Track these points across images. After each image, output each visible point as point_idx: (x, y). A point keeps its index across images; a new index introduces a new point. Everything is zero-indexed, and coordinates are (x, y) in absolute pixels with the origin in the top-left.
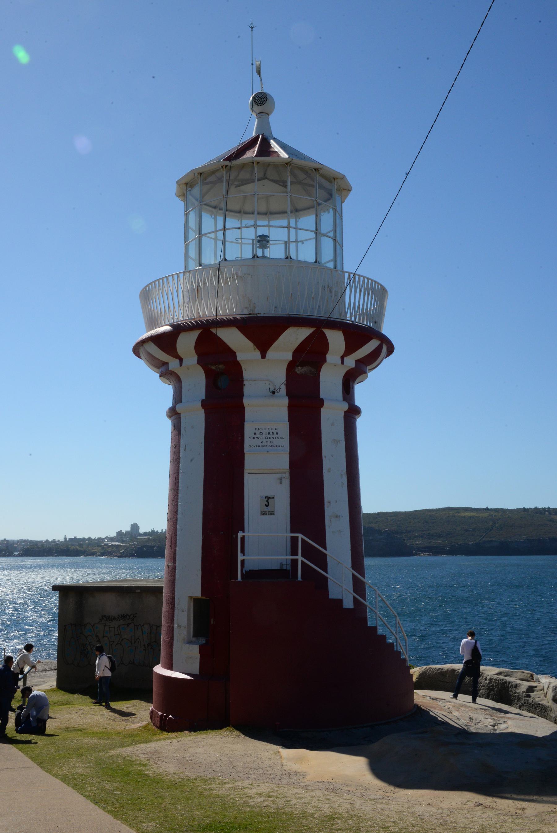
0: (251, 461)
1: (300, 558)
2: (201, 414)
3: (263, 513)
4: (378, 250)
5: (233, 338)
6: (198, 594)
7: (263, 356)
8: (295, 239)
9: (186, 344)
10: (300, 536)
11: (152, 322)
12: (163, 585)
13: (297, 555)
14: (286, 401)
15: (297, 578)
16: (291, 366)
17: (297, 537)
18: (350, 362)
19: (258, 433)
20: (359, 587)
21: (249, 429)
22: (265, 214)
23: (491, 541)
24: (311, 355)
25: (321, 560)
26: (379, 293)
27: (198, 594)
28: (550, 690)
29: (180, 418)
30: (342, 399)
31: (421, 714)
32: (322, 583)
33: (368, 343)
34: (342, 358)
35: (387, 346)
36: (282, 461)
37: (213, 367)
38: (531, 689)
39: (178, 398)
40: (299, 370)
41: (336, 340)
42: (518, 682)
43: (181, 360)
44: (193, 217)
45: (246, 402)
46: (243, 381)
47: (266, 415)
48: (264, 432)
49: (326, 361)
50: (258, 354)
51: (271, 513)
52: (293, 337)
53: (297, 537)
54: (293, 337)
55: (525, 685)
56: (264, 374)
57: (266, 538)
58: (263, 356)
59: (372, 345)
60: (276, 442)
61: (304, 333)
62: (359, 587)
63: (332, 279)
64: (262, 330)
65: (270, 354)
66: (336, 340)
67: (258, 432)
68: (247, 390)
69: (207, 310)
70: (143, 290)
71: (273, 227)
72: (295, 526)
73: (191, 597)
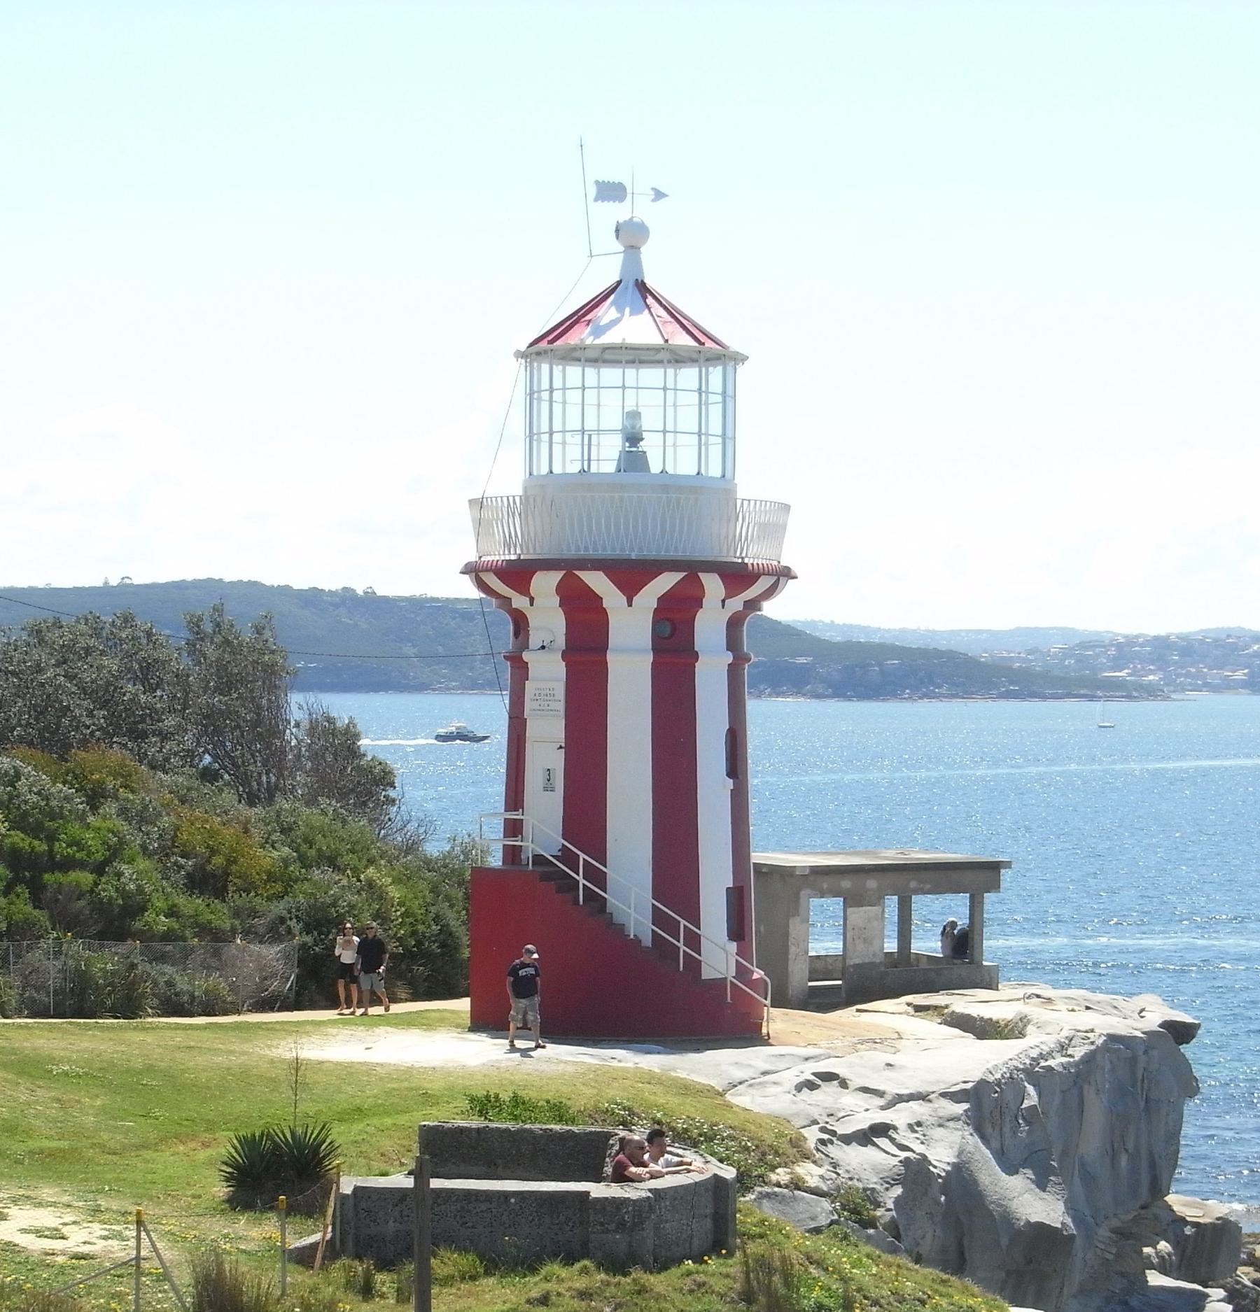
3: (546, 789)
5: (597, 582)
7: (630, 605)
34: (723, 601)
41: (713, 585)
43: (532, 600)
52: (665, 582)
54: (665, 582)
56: (630, 624)
58: (630, 605)
64: (631, 576)
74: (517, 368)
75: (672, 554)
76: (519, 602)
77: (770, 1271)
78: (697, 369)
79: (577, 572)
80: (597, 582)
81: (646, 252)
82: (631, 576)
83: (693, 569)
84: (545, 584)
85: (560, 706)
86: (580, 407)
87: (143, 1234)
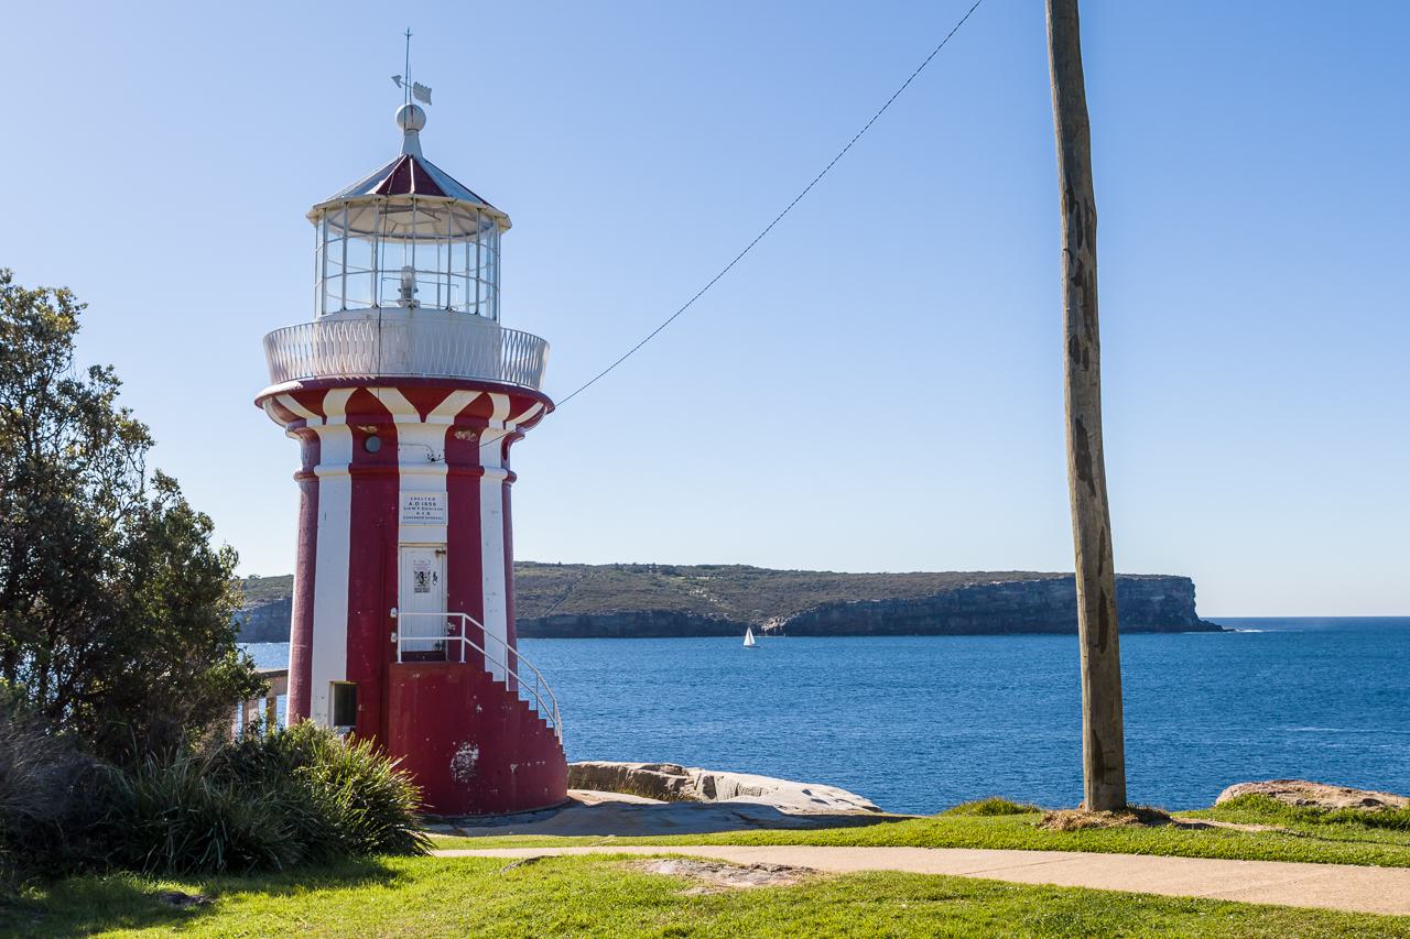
0: (405, 533)
1: (464, 639)
2: (347, 479)
3: (417, 591)
4: (540, 295)
5: (391, 399)
6: (342, 678)
7: (423, 420)
8: (440, 272)
9: (336, 402)
10: (464, 616)
11: (279, 372)
12: (1074, 570)
13: (460, 635)
14: (445, 469)
15: (460, 659)
16: (451, 431)
17: (461, 617)
18: (512, 426)
19: (414, 502)
20: (512, 661)
21: (404, 498)
22: (402, 237)
23: (564, 615)
24: (475, 419)
25: (476, 635)
26: (537, 346)
27: (342, 678)
28: (701, 781)
29: (318, 482)
30: (500, 466)
31: (573, 803)
32: (476, 659)
33: (527, 402)
34: (505, 422)
35: (549, 405)
36: (440, 535)
37: (364, 429)
38: (680, 783)
39: (313, 455)
40: (460, 435)
41: (502, 404)
42: (666, 775)
43: (325, 418)
44: (335, 250)
45: (401, 468)
46: (397, 444)
47: (422, 484)
48: (420, 502)
49: (488, 426)
50: (417, 417)
51: (426, 591)
52: (460, 400)
53: (461, 617)
54: (460, 400)
55: (672, 779)
56: (421, 440)
57: (419, 618)
58: (423, 420)
59: (538, 406)
60: (433, 513)
61: (469, 397)
62: (512, 661)
63: (484, 328)
64: (426, 394)
65: (430, 417)
66: (502, 404)
67: (414, 502)
68: (401, 455)
69: (356, 365)
70: (268, 335)
71: (439, 288)
72: (452, 605)
73: (332, 683)
74: (310, 234)
75: (467, 376)
76: (313, 421)
77: (228, 641)
78: (464, 245)
79: (373, 391)
80: (391, 399)
81: (423, 135)
82: (426, 394)
83: (486, 388)
84: (336, 402)
85: (444, 514)
86: (348, 297)
87: (467, 215)
